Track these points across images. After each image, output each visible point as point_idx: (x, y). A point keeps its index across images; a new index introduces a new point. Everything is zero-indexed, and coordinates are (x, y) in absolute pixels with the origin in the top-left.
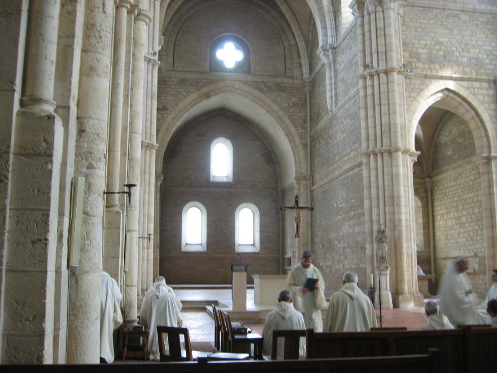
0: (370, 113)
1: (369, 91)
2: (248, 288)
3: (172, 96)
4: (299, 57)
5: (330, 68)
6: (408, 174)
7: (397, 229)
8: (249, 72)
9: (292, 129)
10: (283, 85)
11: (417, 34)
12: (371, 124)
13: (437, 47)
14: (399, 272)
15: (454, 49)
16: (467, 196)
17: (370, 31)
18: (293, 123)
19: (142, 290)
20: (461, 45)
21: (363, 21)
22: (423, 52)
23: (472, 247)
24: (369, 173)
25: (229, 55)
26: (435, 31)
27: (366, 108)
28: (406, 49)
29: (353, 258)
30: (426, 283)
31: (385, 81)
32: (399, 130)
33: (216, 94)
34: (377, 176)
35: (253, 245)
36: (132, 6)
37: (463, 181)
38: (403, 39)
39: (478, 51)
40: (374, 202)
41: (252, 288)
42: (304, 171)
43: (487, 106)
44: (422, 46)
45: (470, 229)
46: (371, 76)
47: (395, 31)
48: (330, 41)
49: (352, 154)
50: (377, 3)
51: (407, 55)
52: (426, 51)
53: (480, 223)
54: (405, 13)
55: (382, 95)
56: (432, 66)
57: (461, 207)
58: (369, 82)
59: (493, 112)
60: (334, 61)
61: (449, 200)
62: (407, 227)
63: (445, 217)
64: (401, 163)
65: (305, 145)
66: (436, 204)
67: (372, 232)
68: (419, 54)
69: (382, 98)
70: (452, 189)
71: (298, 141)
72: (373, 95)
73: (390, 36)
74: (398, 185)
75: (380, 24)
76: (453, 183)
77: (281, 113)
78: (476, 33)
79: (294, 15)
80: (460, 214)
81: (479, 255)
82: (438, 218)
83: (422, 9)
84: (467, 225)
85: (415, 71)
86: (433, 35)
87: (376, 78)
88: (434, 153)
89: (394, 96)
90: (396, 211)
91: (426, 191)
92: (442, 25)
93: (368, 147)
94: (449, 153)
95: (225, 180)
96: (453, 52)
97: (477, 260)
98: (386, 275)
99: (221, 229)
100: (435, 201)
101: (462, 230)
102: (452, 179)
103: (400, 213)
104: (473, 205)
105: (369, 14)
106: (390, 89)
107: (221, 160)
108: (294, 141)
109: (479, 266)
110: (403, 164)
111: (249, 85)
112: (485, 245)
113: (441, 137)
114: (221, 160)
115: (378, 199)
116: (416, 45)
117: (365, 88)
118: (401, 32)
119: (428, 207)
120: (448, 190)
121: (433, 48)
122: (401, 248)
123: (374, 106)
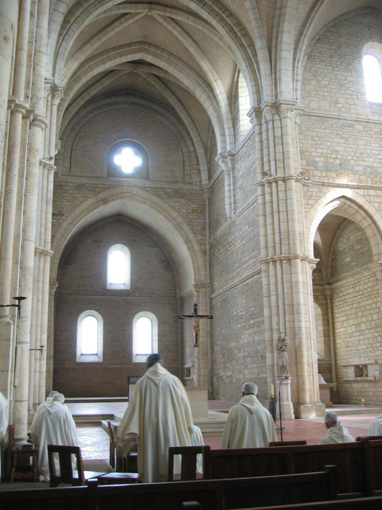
0: (269, 221)
3: (68, 201)
4: (198, 164)
5: (229, 175)
7: (297, 337)
9: (191, 236)
10: (182, 191)
12: (269, 232)
13: (334, 156)
14: (300, 381)
15: (349, 158)
17: (268, 139)
18: (192, 229)
22: (320, 161)
25: (127, 160)
26: (331, 140)
28: (303, 157)
29: (254, 368)
30: (328, 392)
31: (284, 189)
32: (298, 237)
33: (113, 200)
34: (276, 284)
36: (28, 111)
39: (372, 160)
42: (202, 278)
44: (319, 155)
45: (369, 336)
46: (270, 183)
48: (228, 148)
50: (274, 112)
51: (304, 163)
52: (322, 159)
55: (280, 202)
56: (329, 174)
57: (360, 314)
58: (267, 190)
60: (233, 168)
64: (300, 270)
65: (204, 252)
66: (336, 311)
68: (317, 162)
71: (197, 248)
72: (272, 202)
75: (278, 133)
77: (179, 219)
78: (370, 143)
79: (193, 121)
83: (318, 118)
84: (367, 332)
86: (329, 144)
87: (274, 185)
90: (296, 319)
91: (326, 299)
92: (338, 134)
94: (348, 260)
95: (122, 287)
99: (117, 338)
100: (335, 308)
101: (362, 337)
103: (299, 321)
104: (372, 312)
105: (267, 123)
106: (290, 219)
108: (192, 247)
111: (148, 191)
113: (339, 244)
114: (118, 267)
115: (278, 307)
117: (264, 195)
120: (347, 297)
122: (302, 357)
123: (272, 213)
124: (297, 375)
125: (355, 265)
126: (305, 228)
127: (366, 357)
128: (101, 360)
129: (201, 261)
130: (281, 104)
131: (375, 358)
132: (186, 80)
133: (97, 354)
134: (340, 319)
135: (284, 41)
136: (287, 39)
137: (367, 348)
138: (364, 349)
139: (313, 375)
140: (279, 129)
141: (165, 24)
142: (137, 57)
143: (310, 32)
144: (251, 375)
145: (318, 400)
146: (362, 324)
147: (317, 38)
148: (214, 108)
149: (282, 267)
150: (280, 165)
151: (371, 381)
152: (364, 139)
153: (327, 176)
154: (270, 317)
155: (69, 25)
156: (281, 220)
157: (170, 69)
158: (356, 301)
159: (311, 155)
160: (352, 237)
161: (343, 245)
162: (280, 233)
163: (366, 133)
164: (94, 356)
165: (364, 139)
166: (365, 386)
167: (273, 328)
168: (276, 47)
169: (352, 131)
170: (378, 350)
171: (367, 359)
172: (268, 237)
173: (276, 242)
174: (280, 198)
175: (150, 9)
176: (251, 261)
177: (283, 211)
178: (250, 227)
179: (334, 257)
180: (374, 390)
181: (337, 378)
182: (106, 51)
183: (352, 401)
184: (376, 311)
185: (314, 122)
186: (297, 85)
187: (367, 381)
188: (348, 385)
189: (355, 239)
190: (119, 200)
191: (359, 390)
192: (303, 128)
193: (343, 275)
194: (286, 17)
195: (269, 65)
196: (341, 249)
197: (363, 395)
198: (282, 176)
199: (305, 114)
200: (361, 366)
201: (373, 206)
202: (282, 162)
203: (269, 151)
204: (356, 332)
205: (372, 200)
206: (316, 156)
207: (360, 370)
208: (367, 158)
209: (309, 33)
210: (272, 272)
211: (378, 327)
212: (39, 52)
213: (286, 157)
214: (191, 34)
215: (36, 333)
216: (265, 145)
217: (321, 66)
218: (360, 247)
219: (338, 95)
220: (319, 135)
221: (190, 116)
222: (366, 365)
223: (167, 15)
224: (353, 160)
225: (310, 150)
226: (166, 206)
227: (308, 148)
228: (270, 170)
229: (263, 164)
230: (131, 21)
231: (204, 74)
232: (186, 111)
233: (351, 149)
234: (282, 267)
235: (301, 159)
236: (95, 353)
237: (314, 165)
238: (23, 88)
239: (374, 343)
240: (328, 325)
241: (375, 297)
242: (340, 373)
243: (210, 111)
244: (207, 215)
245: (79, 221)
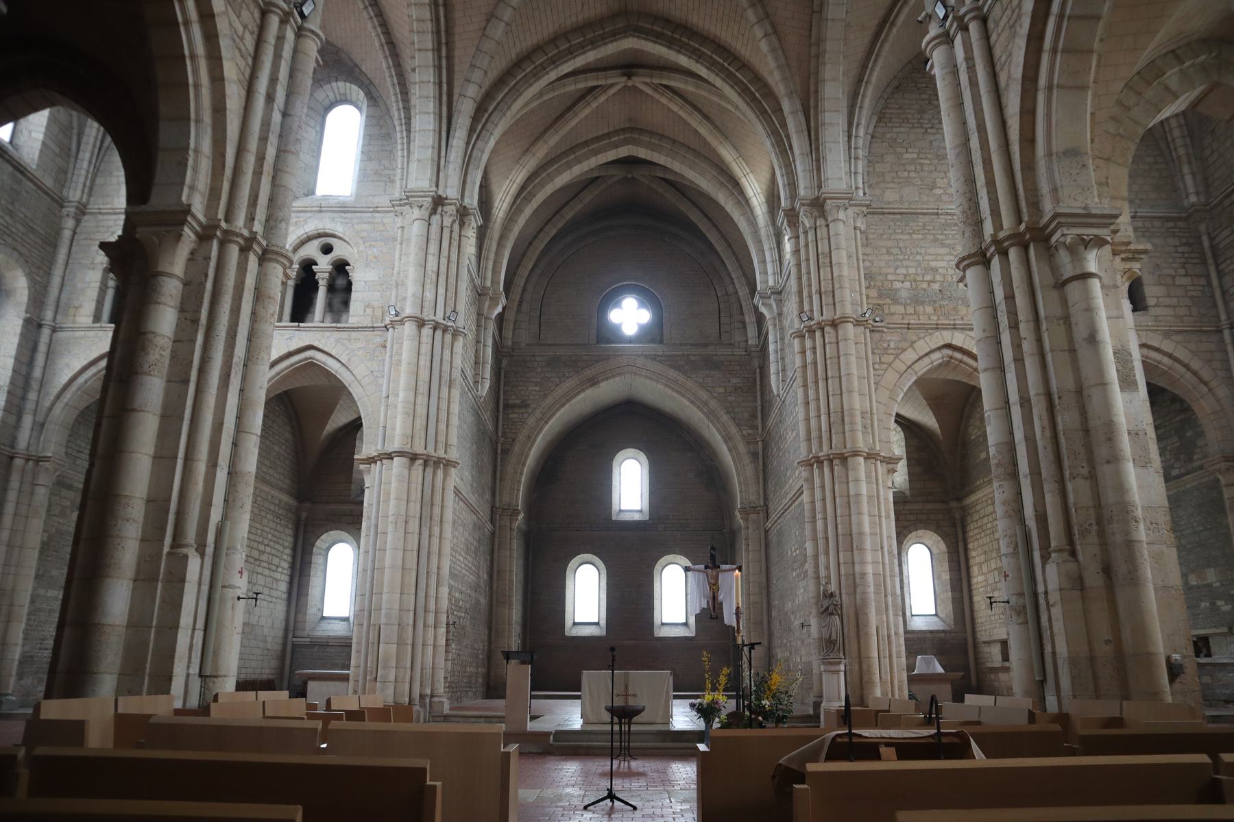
0: (811, 393)
2: (676, 697)
3: (536, 384)
4: (742, 314)
5: (775, 326)
7: (859, 590)
8: (661, 342)
9: (733, 430)
10: (716, 358)
12: (812, 414)
13: (928, 278)
14: (865, 667)
17: (808, 260)
18: (734, 419)
19: (421, 695)
21: (797, 244)
22: (904, 290)
24: (813, 495)
25: (630, 316)
26: (923, 251)
31: (834, 340)
32: (859, 419)
33: (607, 379)
34: (824, 500)
35: (686, 624)
36: (246, 239)
41: (578, 697)
42: (753, 497)
44: (901, 278)
46: (812, 332)
47: (849, 257)
48: (771, 283)
50: (816, 214)
51: (873, 293)
52: (907, 284)
54: (868, 226)
55: (828, 362)
56: (920, 309)
58: (808, 343)
60: (780, 314)
62: (877, 585)
63: (985, 569)
64: (863, 475)
65: (754, 455)
66: (970, 546)
71: (742, 448)
72: (815, 363)
75: (823, 247)
77: (713, 404)
79: (730, 246)
82: (975, 570)
83: (899, 217)
85: (888, 319)
86: (919, 258)
87: (818, 334)
90: (857, 559)
91: (954, 525)
93: (810, 451)
95: (637, 517)
99: (630, 597)
103: (863, 563)
105: (806, 233)
107: (631, 485)
108: (735, 448)
111: (660, 362)
113: (970, 429)
114: (631, 485)
115: (827, 539)
116: (890, 277)
117: (803, 352)
118: (861, 257)
120: (985, 520)
122: (867, 624)
123: (817, 382)
124: (860, 657)
126: (874, 404)
128: (604, 633)
129: (749, 470)
130: (825, 199)
132: (704, 182)
133: (597, 624)
134: (978, 560)
135: (826, 96)
136: (833, 92)
140: (826, 241)
141: (657, 96)
142: (623, 152)
143: (877, 76)
147: (895, 84)
148: (748, 220)
149: (832, 471)
150: (827, 300)
153: (915, 312)
154: (816, 557)
155: (486, 115)
157: (676, 166)
164: (594, 627)
168: (816, 107)
175: (629, 76)
182: (572, 150)
186: (856, 167)
188: (993, 677)
190: (617, 379)
192: (871, 236)
194: (827, 56)
195: (807, 138)
198: (830, 318)
199: (871, 211)
203: (809, 279)
208: (1103, 287)
209: (874, 79)
212: (285, 151)
213: (837, 286)
214: (700, 106)
215: (427, 586)
217: (902, 130)
219: (935, 175)
220: (901, 245)
221: (724, 237)
223: (656, 81)
225: (884, 271)
226: (690, 384)
230: (602, 99)
231: (727, 167)
232: (718, 230)
234: (832, 471)
236: (596, 620)
237: (890, 294)
238: (245, 205)
240: (960, 570)
243: (742, 224)
244: (759, 394)
245: (554, 414)
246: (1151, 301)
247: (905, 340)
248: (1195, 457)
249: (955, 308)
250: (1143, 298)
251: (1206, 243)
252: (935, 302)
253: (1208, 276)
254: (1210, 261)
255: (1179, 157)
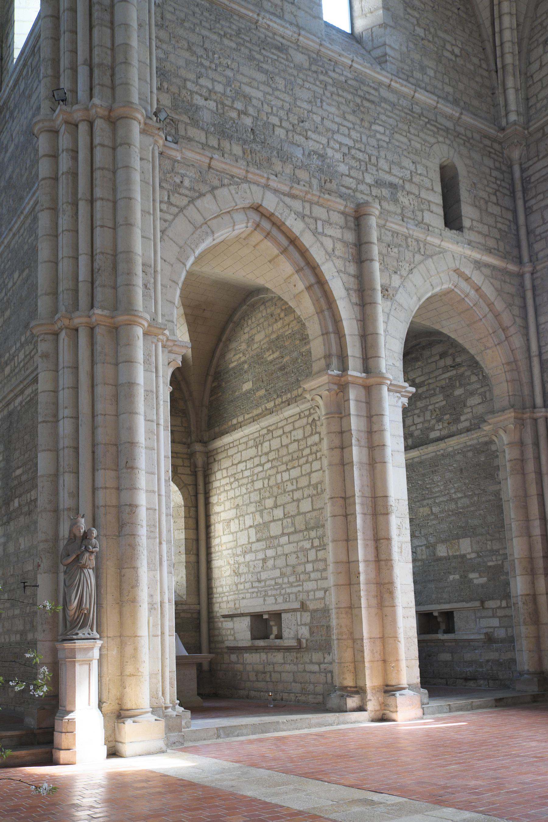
0: (64, 222)
1: (65, 163)
6: (157, 392)
11: (194, 59)
12: (64, 251)
13: (239, 105)
15: (275, 120)
16: (286, 476)
20: (291, 115)
23: (295, 590)
26: (234, 66)
27: (54, 209)
28: (165, 85)
29: (14, 617)
30: (192, 673)
34: (76, 388)
37: (276, 443)
38: (158, 59)
39: (324, 141)
40: (66, 457)
43: (339, 263)
45: (288, 549)
49: (21, 355)
51: (166, 101)
52: (212, 105)
53: (313, 534)
55: (98, 174)
56: (226, 144)
57: (269, 503)
59: (352, 279)
61: (244, 490)
64: (140, 355)
66: (214, 499)
67: (56, 538)
68: (198, 108)
69: (98, 182)
70: (249, 464)
72: (75, 174)
73: (127, 26)
74: (132, 413)
76: (252, 452)
78: (322, 101)
80: (267, 518)
81: (312, 606)
84: (284, 540)
86: (229, 73)
88: (214, 391)
89: (128, 181)
91: (195, 474)
92: (251, 58)
94: (247, 386)
96: (274, 126)
97: (307, 617)
98: (89, 663)
100: (213, 492)
101: (270, 553)
102: (251, 443)
104: (297, 495)
106: (120, 220)
109: (311, 633)
110: (146, 361)
112: (331, 581)
113: (230, 355)
116: (189, 85)
119: (196, 507)
121: (228, 102)
123: (75, 204)
125: (261, 398)
127: (281, 594)
131: (302, 597)
134: (223, 516)
137: (283, 575)
138: (274, 579)
139: (163, 633)
144: (7, 637)
145: (172, 702)
146: (272, 524)
151: (288, 649)
152: (309, 89)
156: (98, 223)
158: (261, 475)
159: (185, 87)
160: (258, 338)
161: (237, 357)
162: (92, 256)
163: (315, 75)
165: (309, 89)
166: (275, 660)
167: (61, 507)
169: (282, 61)
170: (309, 580)
171: (280, 600)
172: (60, 265)
173: (81, 278)
174: (98, 163)
176: (21, 355)
177: (102, 199)
178: (23, 271)
179: (215, 384)
180: (294, 668)
181: (210, 642)
183: (242, 693)
184: (307, 492)
185: (197, 10)
187: (279, 649)
188: (234, 657)
189: (267, 339)
191: (260, 668)
192: (168, 16)
193: (235, 421)
196: (232, 365)
197: (268, 679)
200: (266, 617)
201: (322, 244)
202: (109, 73)
203: (74, 42)
204: (258, 541)
205: (320, 230)
206: (197, 93)
207: (264, 625)
210: (65, 357)
211: (312, 529)
216: (64, 25)
218: (277, 354)
222: (280, 614)
224: (281, 126)
225: (183, 72)
227: (179, 68)
228: (74, 91)
229: (57, 76)
233: (280, 103)
235: (159, 89)
239: (299, 564)
241: (307, 462)
242: (216, 632)
246: (466, 223)
247: (204, 181)
248: (462, 418)
249: (269, 159)
250: (459, 217)
251: (517, 174)
252: (245, 142)
253: (515, 212)
254: (519, 194)
255: (504, 67)
